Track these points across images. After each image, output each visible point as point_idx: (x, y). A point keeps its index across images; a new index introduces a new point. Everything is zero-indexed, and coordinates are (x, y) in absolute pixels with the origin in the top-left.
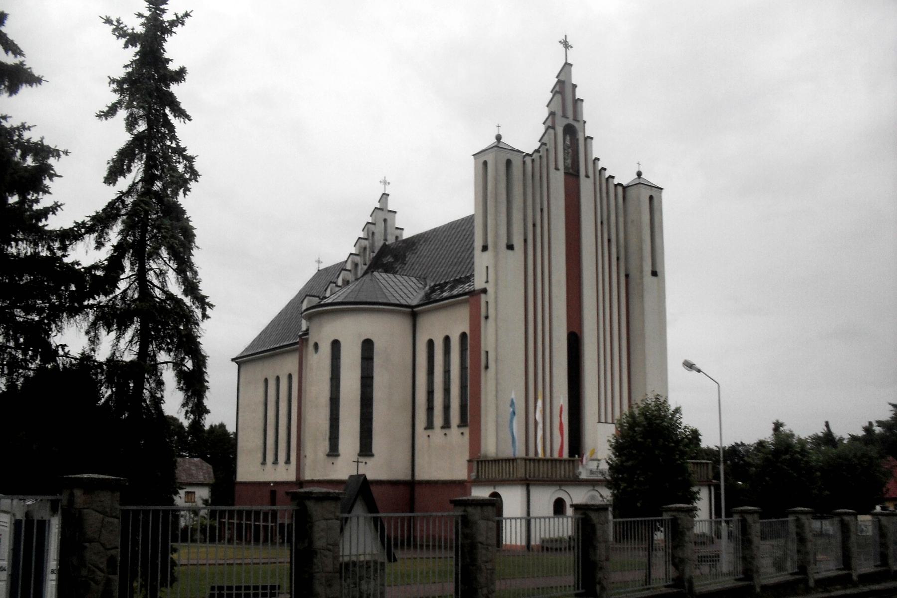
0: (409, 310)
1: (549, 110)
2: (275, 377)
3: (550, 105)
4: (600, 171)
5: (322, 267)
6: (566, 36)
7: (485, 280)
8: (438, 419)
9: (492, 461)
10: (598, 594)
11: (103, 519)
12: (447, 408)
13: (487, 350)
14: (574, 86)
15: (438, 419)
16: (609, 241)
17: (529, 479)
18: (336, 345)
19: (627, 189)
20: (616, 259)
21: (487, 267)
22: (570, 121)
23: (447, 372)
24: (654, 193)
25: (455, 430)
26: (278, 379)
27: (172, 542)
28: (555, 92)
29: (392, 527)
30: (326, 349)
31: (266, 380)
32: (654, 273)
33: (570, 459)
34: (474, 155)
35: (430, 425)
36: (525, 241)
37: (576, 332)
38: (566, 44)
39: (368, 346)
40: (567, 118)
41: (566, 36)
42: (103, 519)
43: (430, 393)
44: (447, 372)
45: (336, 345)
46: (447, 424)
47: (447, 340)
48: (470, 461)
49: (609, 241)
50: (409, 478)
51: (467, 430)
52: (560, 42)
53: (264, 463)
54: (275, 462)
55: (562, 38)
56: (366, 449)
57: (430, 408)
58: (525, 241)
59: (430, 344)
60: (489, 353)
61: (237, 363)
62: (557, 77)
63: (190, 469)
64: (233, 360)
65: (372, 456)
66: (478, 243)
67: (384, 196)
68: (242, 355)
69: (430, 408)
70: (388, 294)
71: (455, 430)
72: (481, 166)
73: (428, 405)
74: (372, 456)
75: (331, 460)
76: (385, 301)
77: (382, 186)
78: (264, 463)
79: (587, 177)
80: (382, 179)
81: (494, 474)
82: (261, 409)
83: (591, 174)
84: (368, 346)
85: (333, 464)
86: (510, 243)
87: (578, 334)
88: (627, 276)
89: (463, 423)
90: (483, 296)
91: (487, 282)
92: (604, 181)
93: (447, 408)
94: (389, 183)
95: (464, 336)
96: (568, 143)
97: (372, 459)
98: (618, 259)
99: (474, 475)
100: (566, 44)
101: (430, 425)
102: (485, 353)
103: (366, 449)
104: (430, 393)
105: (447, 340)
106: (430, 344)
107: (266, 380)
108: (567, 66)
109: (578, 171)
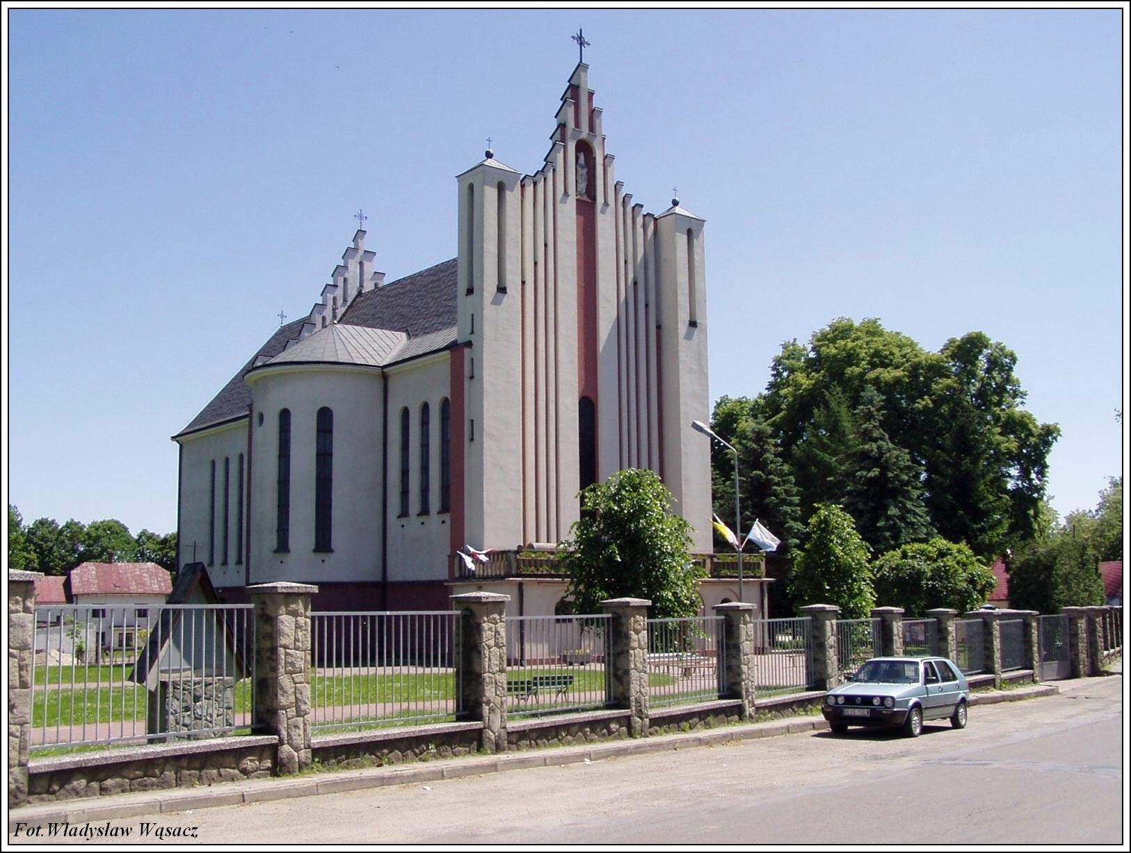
1: (557, 121)
2: (224, 459)
3: (558, 117)
5: (286, 322)
6: (581, 30)
7: (470, 331)
11: (989, 600)
12: (425, 490)
13: (472, 419)
14: (591, 94)
18: (285, 416)
20: (644, 306)
21: (473, 315)
23: (425, 446)
25: (434, 518)
26: (227, 460)
30: (272, 422)
31: (213, 463)
34: (456, 177)
35: (404, 513)
38: (581, 41)
39: (325, 418)
41: (581, 30)
42: (989, 600)
43: (405, 473)
44: (425, 446)
45: (285, 416)
46: (425, 511)
47: (425, 408)
50: (379, 578)
51: (447, 517)
52: (573, 37)
55: (576, 33)
56: (323, 544)
57: (405, 493)
59: (406, 413)
60: (474, 422)
61: (178, 442)
62: (569, 81)
63: (141, 576)
64: (173, 438)
66: (462, 286)
67: (359, 233)
68: (185, 432)
69: (405, 493)
70: (350, 349)
71: (434, 518)
72: (466, 191)
73: (403, 488)
74: (332, 551)
75: (280, 557)
82: (207, 498)
84: (325, 418)
85: (282, 562)
86: (693, 320)
87: (592, 398)
88: (659, 327)
89: (444, 509)
90: (467, 351)
91: (472, 332)
92: (630, 209)
93: (425, 490)
94: (366, 218)
95: (445, 403)
98: (647, 306)
100: (581, 41)
101: (404, 513)
103: (323, 544)
104: (405, 473)
105: (425, 408)
106: (406, 413)
107: (213, 463)
108: (581, 67)
109: (594, 198)
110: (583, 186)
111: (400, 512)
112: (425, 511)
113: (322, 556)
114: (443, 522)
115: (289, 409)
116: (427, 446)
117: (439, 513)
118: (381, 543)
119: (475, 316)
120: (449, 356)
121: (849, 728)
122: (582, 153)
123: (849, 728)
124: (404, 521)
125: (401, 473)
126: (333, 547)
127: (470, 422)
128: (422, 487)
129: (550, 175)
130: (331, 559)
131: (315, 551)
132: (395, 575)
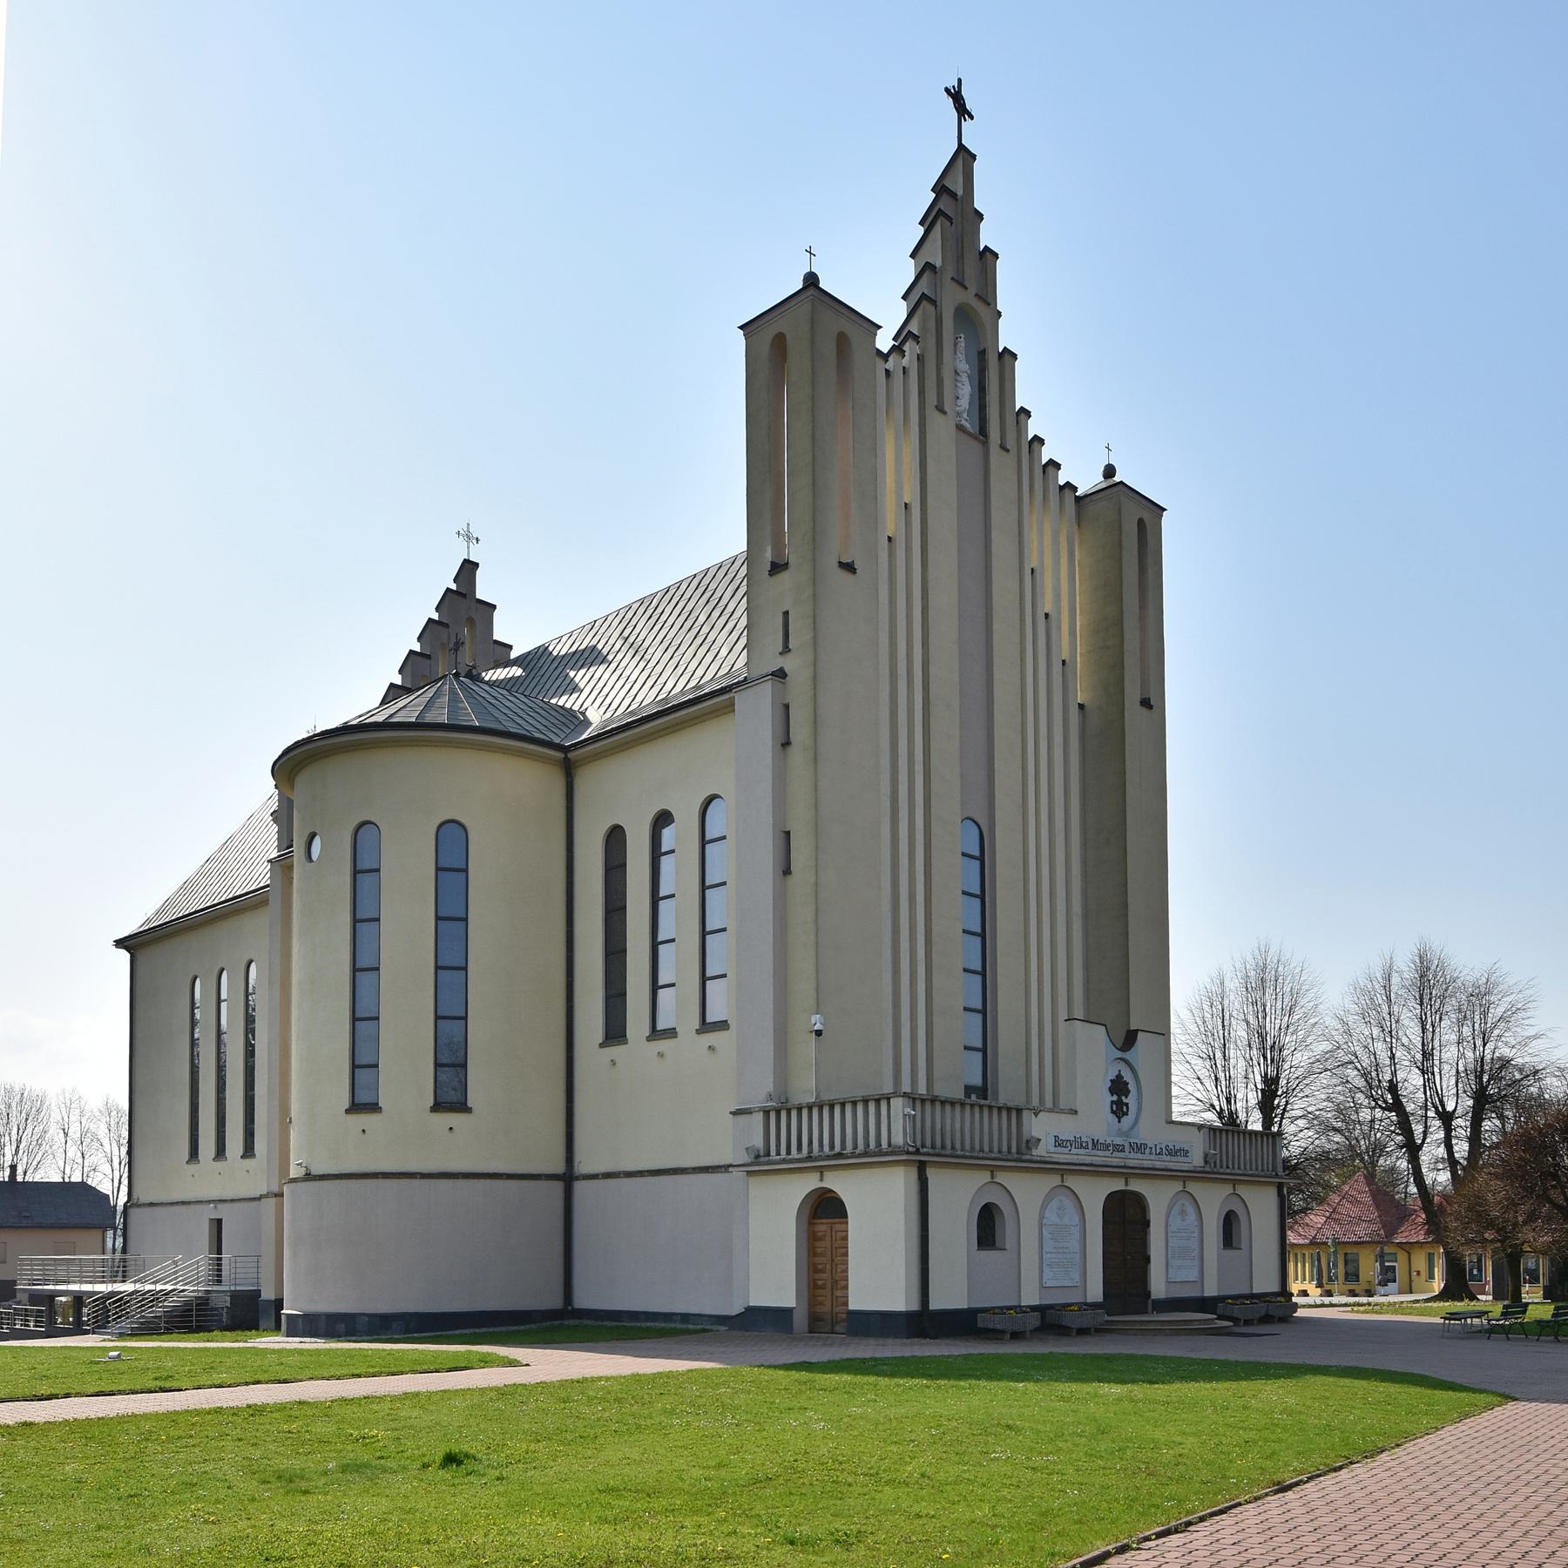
0: (560, 755)
4: (1031, 442)
6: (960, 81)
10: (1189, 1529)
12: (1057, 578)
24: (1146, 517)
28: (930, 220)
29: (633, 1324)
32: (1146, 703)
39: (451, 835)
53: (194, 1154)
54: (220, 1152)
59: (616, 838)
77: (462, 543)
78: (194, 1154)
79: (1003, 447)
80: (462, 527)
81: (250, 1265)
83: (1010, 444)
102: (477, 1092)
106: (616, 838)
108: (963, 157)
118: (357, 989)
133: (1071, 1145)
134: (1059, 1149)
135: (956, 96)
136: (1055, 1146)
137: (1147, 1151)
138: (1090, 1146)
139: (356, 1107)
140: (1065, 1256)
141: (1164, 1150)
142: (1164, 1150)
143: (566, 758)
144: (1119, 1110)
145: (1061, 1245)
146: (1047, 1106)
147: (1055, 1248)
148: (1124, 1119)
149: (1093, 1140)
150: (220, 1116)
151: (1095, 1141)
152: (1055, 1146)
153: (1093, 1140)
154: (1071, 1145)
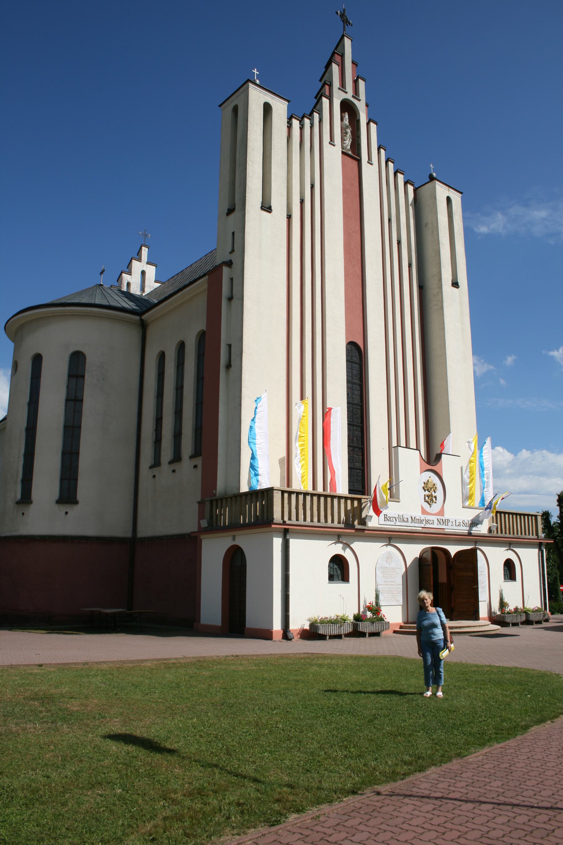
0: (138, 318)
8: (167, 453)
9: (231, 498)
12: (177, 435)
15: (167, 453)
16: (399, 243)
17: (288, 522)
19: (418, 190)
21: (233, 233)
22: (349, 96)
25: (186, 463)
27: (475, 616)
33: (350, 496)
35: (156, 463)
36: (289, 217)
37: (361, 344)
40: (346, 93)
43: (159, 420)
46: (177, 458)
47: (181, 346)
48: (201, 503)
49: (399, 243)
50: (129, 535)
51: (199, 461)
57: (158, 441)
58: (289, 217)
59: (162, 356)
65: (76, 502)
69: (158, 441)
71: (186, 463)
74: (76, 502)
76: (105, 303)
91: (233, 251)
93: (177, 435)
95: (202, 336)
96: (347, 122)
97: (76, 508)
99: (204, 524)
101: (156, 463)
104: (159, 420)
106: (162, 356)
110: (348, 142)
111: (153, 463)
112: (177, 458)
113: (67, 508)
114: (195, 466)
115: (43, 355)
116: (182, 387)
117: (191, 457)
118: (132, 497)
119: (219, 104)
120: (206, 286)
121: (242, 516)
122: (346, 113)
123: (242, 516)
124: (156, 471)
125: (155, 421)
126: (79, 498)
127: (227, 347)
128: (175, 433)
129: (316, 116)
130: (74, 510)
131: (59, 502)
132: (144, 531)
133: (396, 520)
134: (388, 523)
135: (342, 16)
136: (385, 521)
137: (450, 524)
138: (410, 520)
139: (61, 501)
140: (392, 586)
141: (462, 523)
142: (462, 523)
143: (142, 320)
144: (430, 499)
145: (389, 580)
146: (323, 498)
147: (385, 582)
148: (434, 505)
149: (411, 517)
150: (358, 465)
151: (413, 518)
152: (385, 521)
153: (411, 517)
154: (396, 520)
